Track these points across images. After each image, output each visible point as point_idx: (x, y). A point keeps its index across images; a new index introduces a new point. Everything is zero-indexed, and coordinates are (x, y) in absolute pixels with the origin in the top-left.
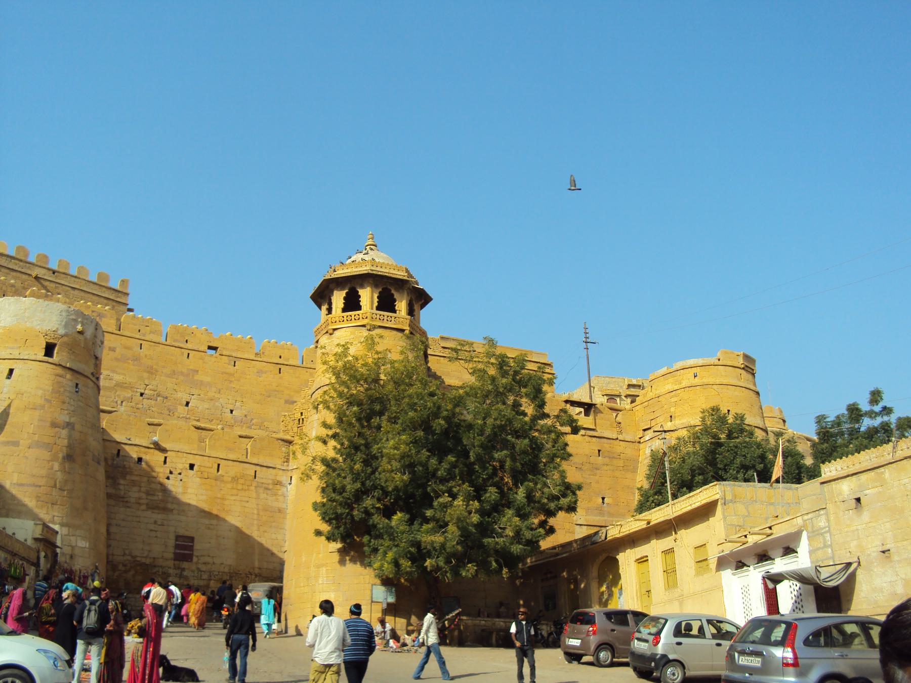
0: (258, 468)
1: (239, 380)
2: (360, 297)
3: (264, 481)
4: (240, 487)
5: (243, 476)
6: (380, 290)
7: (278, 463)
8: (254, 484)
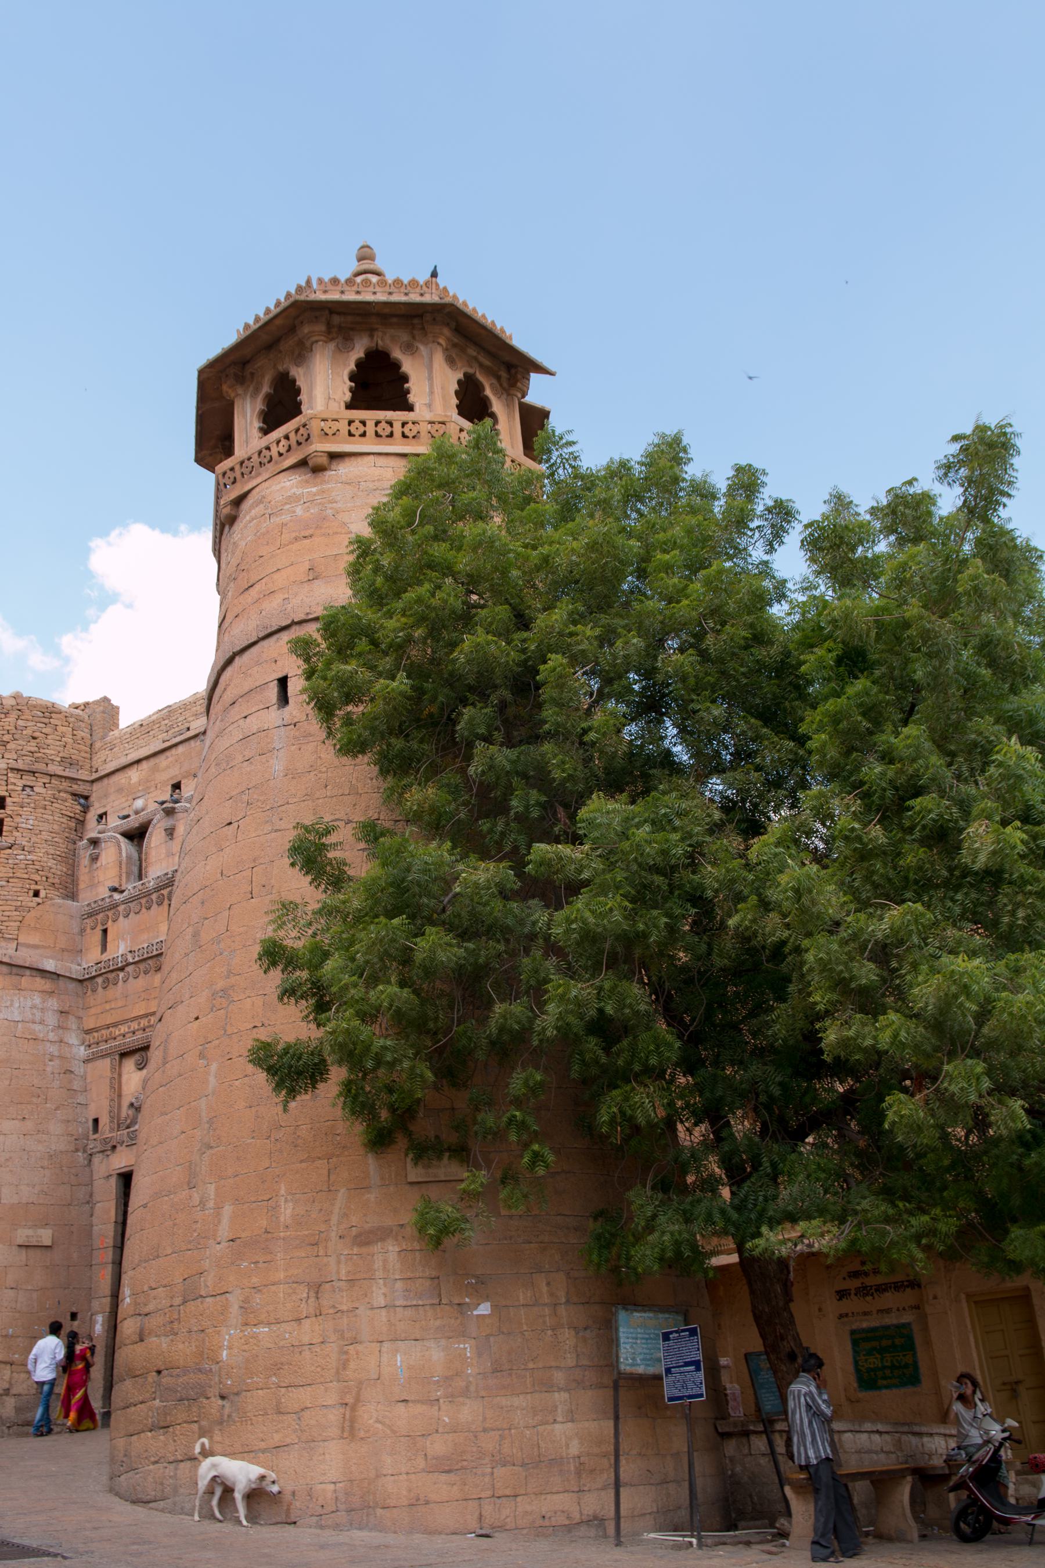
2: (405, 379)
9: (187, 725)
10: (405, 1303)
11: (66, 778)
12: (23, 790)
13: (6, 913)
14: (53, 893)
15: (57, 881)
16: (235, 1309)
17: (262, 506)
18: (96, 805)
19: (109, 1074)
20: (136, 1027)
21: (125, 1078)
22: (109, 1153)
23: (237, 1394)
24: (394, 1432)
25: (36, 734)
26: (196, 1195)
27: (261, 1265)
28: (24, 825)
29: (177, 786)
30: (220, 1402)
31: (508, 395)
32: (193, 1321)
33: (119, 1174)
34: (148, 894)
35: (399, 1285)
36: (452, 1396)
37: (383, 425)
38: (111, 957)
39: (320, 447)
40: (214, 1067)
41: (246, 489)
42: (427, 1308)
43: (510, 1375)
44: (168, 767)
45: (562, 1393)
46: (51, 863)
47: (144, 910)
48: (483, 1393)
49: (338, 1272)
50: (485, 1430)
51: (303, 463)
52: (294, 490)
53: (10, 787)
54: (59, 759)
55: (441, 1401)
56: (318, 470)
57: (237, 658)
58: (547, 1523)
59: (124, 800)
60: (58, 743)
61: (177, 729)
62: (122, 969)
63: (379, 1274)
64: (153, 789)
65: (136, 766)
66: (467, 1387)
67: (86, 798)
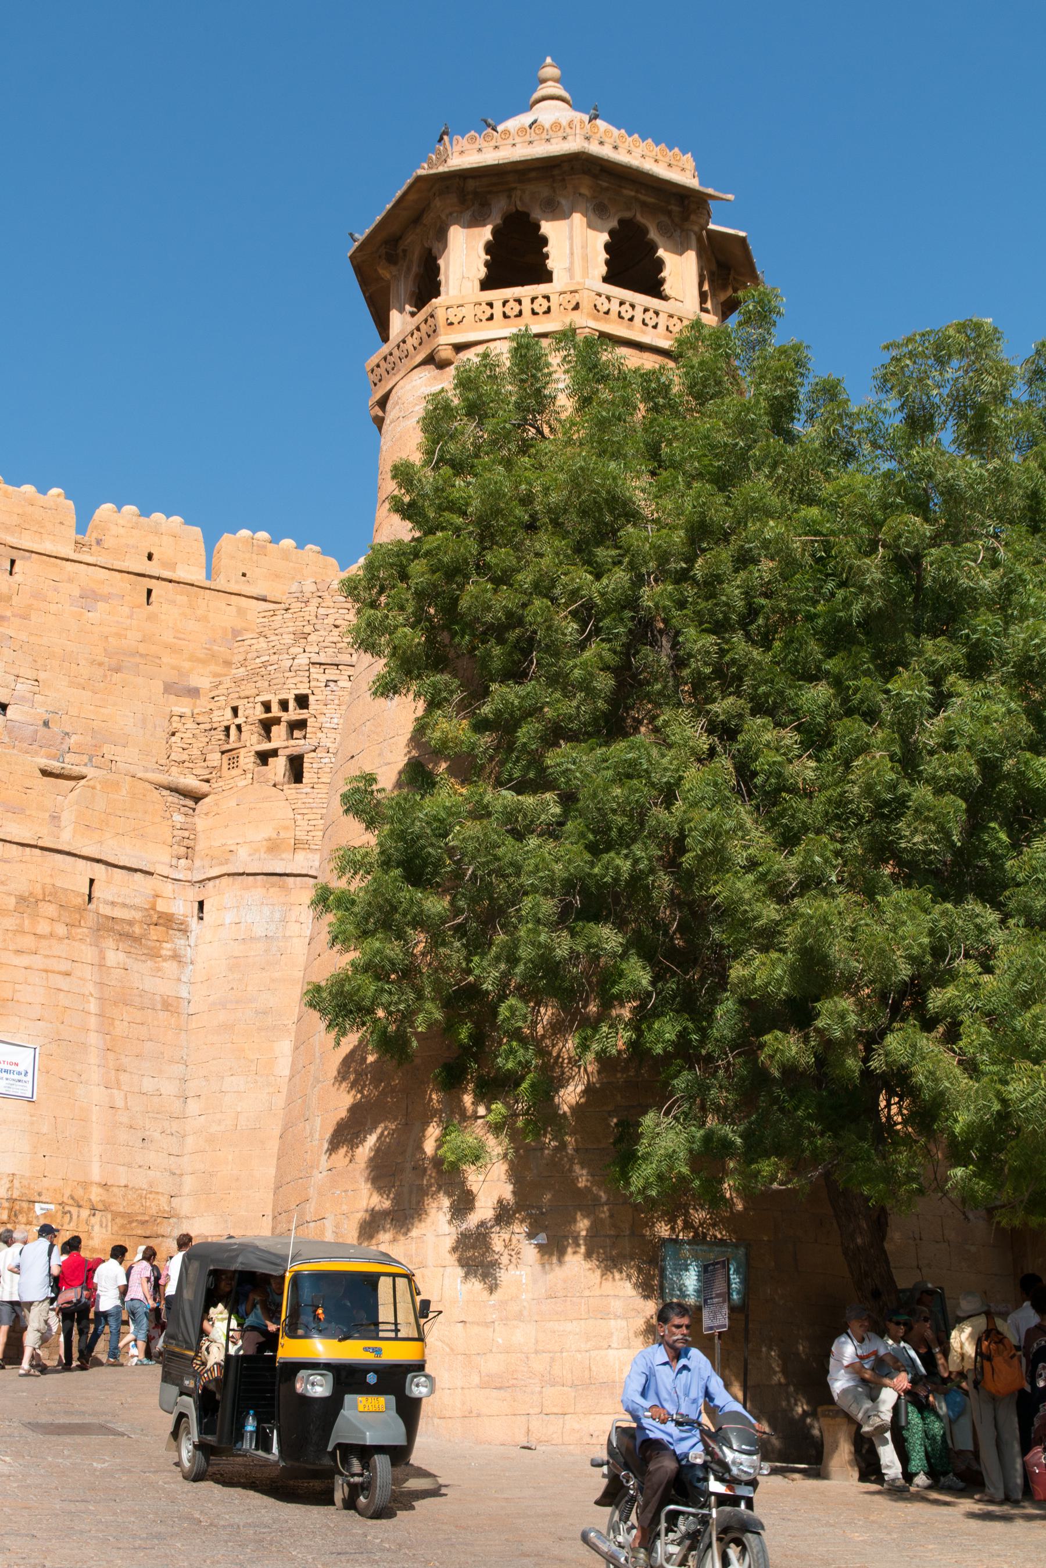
0: (99, 871)
1: (25, 617)
2: (544, 241)
3: (118, 913)
4: (43, 927)
5: (52, 895)
6: (614, 223)
7: (159, 858)
8: (90, 919)
13: (312, 823)
24: (452, 1350)
25: (337, 623)
27: (350, 1193)
31: (682, 230)
37: (512, 304)
48: (536, 1318)
50: (536, 1352)
58: (594, 1441)
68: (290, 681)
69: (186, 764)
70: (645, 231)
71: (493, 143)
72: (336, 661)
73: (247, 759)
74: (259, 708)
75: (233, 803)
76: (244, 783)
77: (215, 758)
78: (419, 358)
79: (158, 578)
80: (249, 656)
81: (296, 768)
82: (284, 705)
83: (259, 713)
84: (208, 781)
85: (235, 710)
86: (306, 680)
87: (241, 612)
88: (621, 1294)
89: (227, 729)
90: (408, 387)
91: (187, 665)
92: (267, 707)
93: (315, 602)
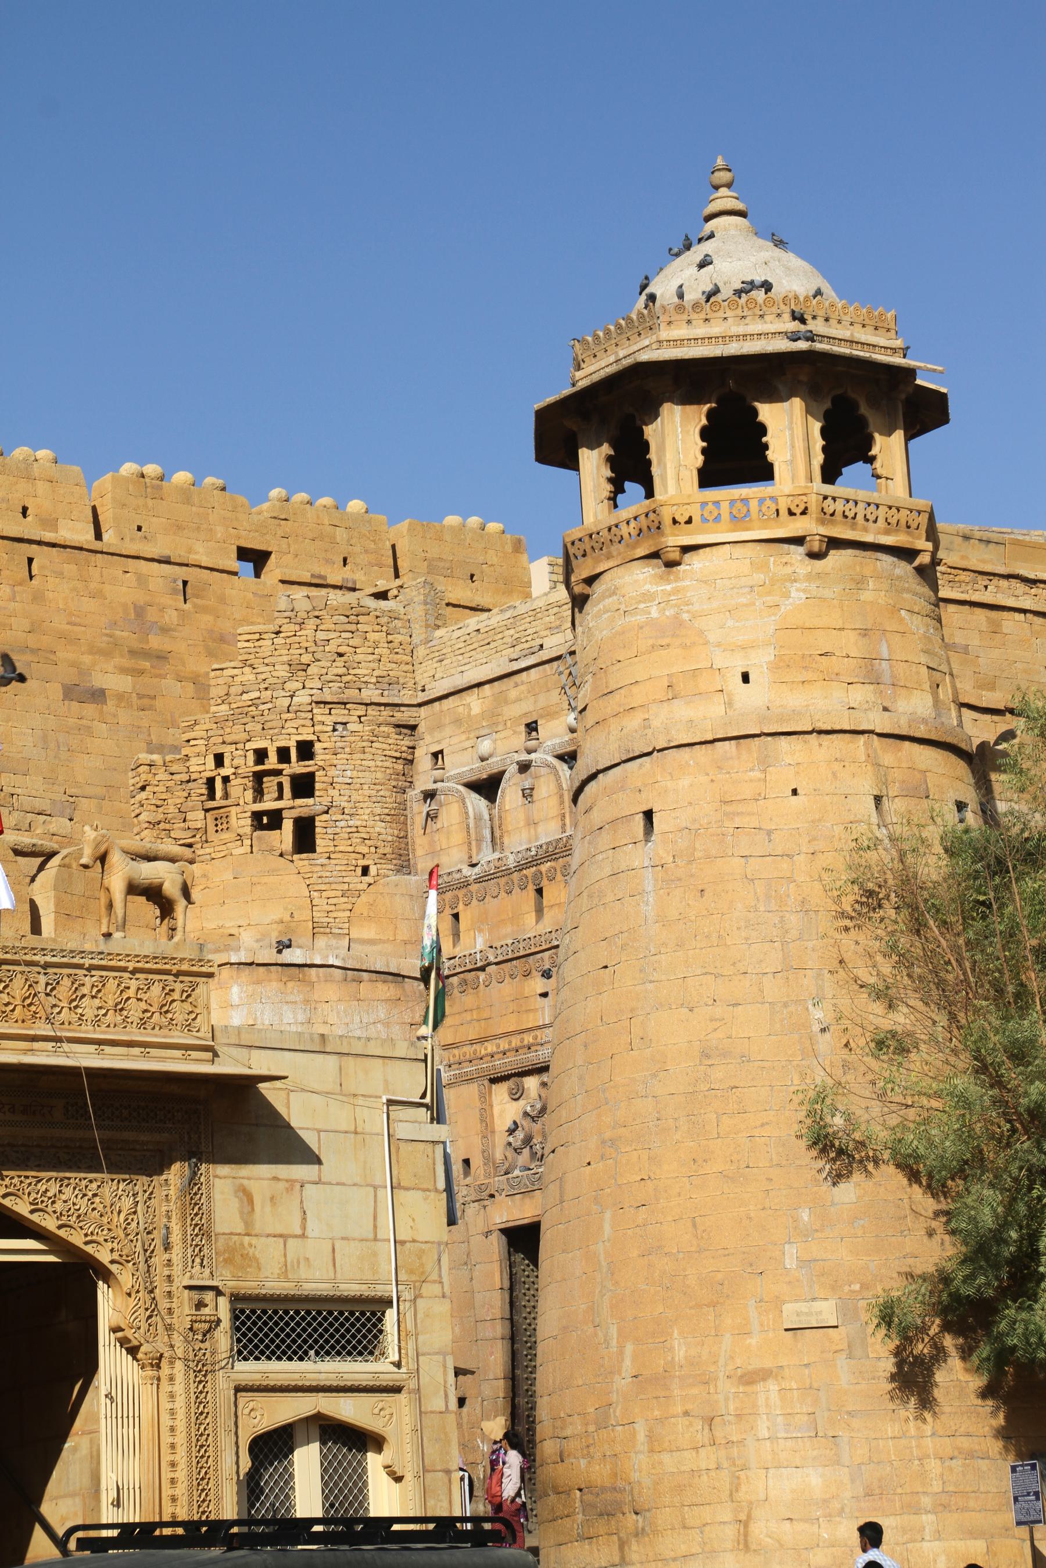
2: (762, 430)
6: (828, 405)
9: (539, 642)
10: (786, 1435)
11: (386, 705)
12: (334, 730)
14: (386, 868)
15: (388, 850)
16: (641, 1437)
17: (615, 598)
18: (428, 739)
19: (478, 1104)
20: (507, 1047)
21: (496, 1110)
22: (486, 1203)
23: (648, 1510)
24: (782, 1546)
25: (341, 650)
26: (600, 1334)
28: (340, 780)
29: (532, 727)
30: (634, 1516)
32: (606, 1446)
33: (504, 1231)
34: (508, 872)
35: (780, 1419)
36: (830, 1516)
38: (467, 953)
39: (674, 539)
40: (608, 1215)
41: (598, 571)
42: (806, 1439)
43: (881, 1498)
44: (518, 700)
45: (929, 1516)
46: (380, 827)
47: (503, 894)
49: (727, 1407)
51: (655, 555)
52: (647, 587)
53: (318, 728)
54: (374, 680)
55: (821, 1520)
56: (671, 564)
57: (600, 776)
59: (464, 737)
60: (371, 658)
61: (526, 646)
62: (482, 969)
63: (762, 1410)
64: (500, 728)
65: (476, 690)
66: (843, 1509)
67: (413, 728)
68: (288, 724)
69: (162, 826)
70: (855, 406)
71: (703, 316)
72: (344, 697)
73: (242, 823)
74: (251, 757)
75: (228, 876)
76: (241, 850)
77: (197, 818)
78: (641, 552)
79: (39, 543)
80: (233, 690)
81: (305, 837)
82: (283, 754)
83: (249, 765)
84: (190, 846)
85: (219, 760)
86: (309, 723)
87: (142, 580)
88: (929, 1491)
89: (210, 782)
90: (627, 579)
91: (87, 659)
92: (261, 755)
93: (311, 623)
